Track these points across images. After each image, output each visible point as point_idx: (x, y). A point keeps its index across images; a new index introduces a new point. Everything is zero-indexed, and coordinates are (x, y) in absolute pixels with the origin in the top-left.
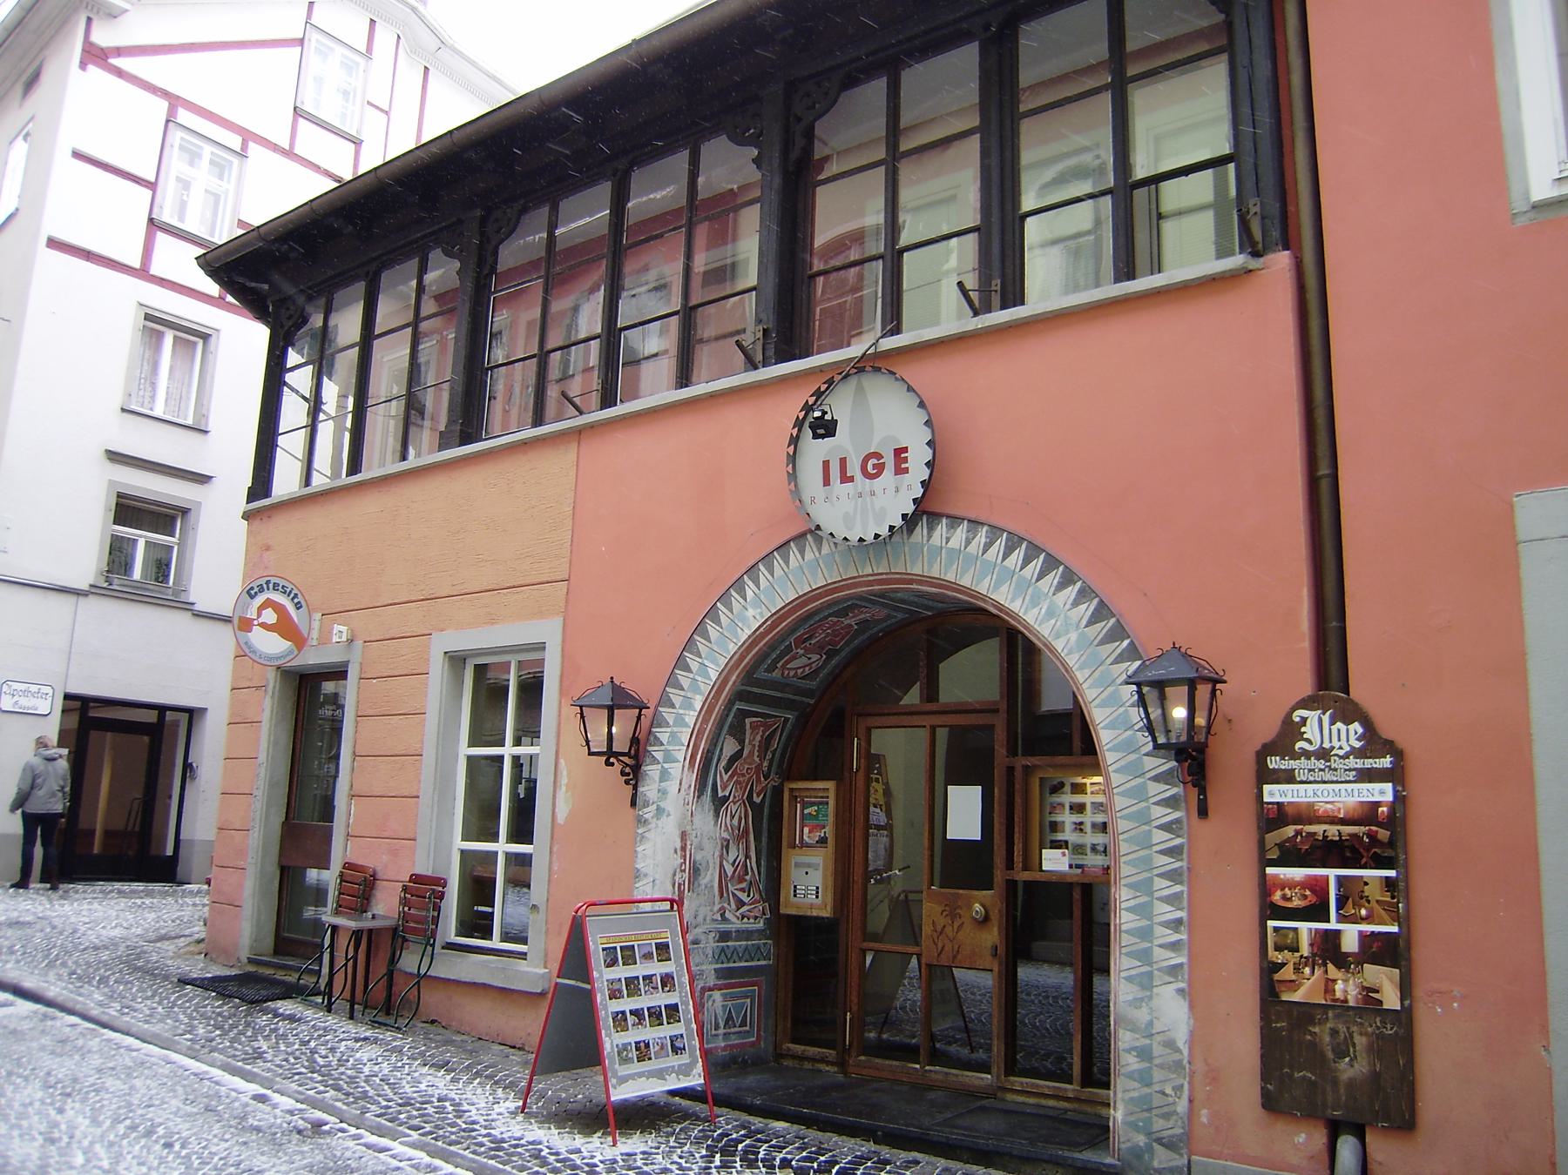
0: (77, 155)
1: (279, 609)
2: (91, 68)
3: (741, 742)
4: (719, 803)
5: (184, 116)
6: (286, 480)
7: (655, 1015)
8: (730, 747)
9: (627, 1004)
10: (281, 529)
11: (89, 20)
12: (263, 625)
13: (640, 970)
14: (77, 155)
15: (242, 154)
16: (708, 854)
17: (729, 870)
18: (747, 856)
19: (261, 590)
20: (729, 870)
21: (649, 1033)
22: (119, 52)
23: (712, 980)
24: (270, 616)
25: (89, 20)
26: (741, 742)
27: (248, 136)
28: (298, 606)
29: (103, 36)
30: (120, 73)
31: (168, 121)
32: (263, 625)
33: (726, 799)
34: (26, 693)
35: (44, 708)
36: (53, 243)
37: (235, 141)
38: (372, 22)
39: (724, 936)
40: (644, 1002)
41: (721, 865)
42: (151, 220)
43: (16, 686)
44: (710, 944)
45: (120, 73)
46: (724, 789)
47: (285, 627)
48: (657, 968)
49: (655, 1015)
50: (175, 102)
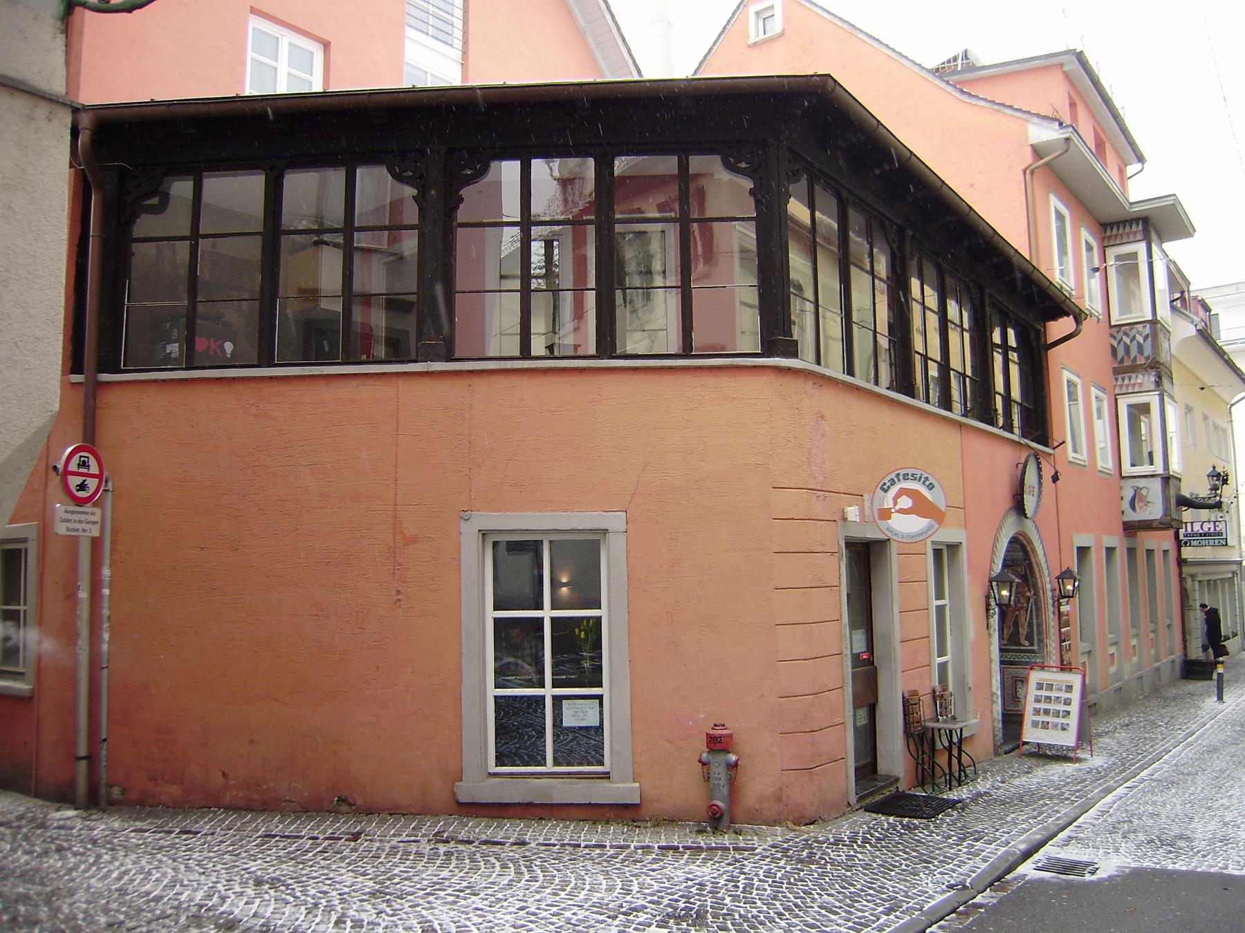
7: (1057, 713)
9: (1042, 706)
12: (902, 511)
13: (1053, 694)
32: (902, 511)
48: (1064, 695)
49: (1057, 713)
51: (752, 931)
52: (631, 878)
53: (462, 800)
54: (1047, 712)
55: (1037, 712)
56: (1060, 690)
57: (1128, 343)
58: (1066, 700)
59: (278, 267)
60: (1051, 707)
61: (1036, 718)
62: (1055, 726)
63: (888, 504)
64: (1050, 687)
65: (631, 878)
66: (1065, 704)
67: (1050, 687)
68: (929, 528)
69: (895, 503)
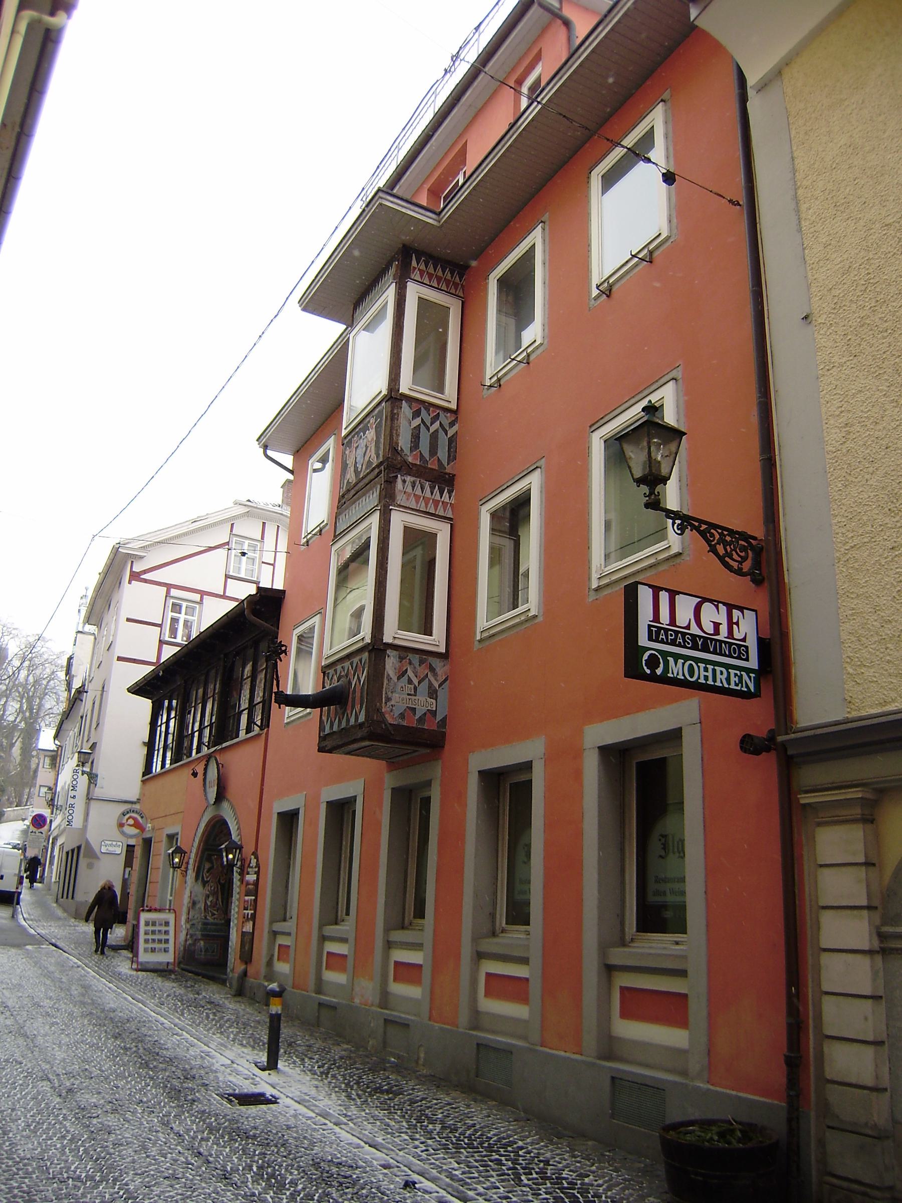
0: (128, 620)
1: (135, 819)
2: (133, 582)
3: (212, 863)
4: (204, 883)
5: (174, 592)
6: (157, 767)
7: (160, 941)
8: (207, 866)
9: (150, 937)
10: (153, 786)
11: (132, 562)
12: (129, 825)
13: (157, 928)
14: (128, 620)
15: (201, 602)
16: (201, 898)
17: (209, 904)
18: (217, 899)
19: (128, 813)
20: (209, 904)
21: (156, 946)
22: (145, 572)
23: (199, 937)
24: (131, 822)
25: (132, 562)
26: (212, 863)
27: (203, 593)
28: (142, 817)
29: (137, 569)
30: (146, 581)
31: (166, 596)
32: (129, 825)
33: (208, 882)
34: (111, 845)
35: (118, 851)
36: (120, 659)
37: (197, 597)
38: (264, 523)
39: (205, 924)
40: (156, 937)
41: (206, 902)
42: (160, 641)
43: (107, 842)
44: (200, 926)
45: (146, 581)
46: (207, 878)
47: (137, 825)
48: (164, 928)
49: (160, 941)
50: (169, 586)
51: (504, 1201)
52: (477, 1164)
53: (754, 613)
54: (154, 940)
55: (166, 932)
56: (161, 925)
57: (436, 685)
58: (165, 932)
59: (401, 341)
60: (156, 937)
61: (147, 946)
62: (160, 950)
63: (124, 821)
64: (154, 924)
65: (477, 1164)
66: (148, 940)
67: (154, 924)
68: (139, 833)
69: (127, 820)
